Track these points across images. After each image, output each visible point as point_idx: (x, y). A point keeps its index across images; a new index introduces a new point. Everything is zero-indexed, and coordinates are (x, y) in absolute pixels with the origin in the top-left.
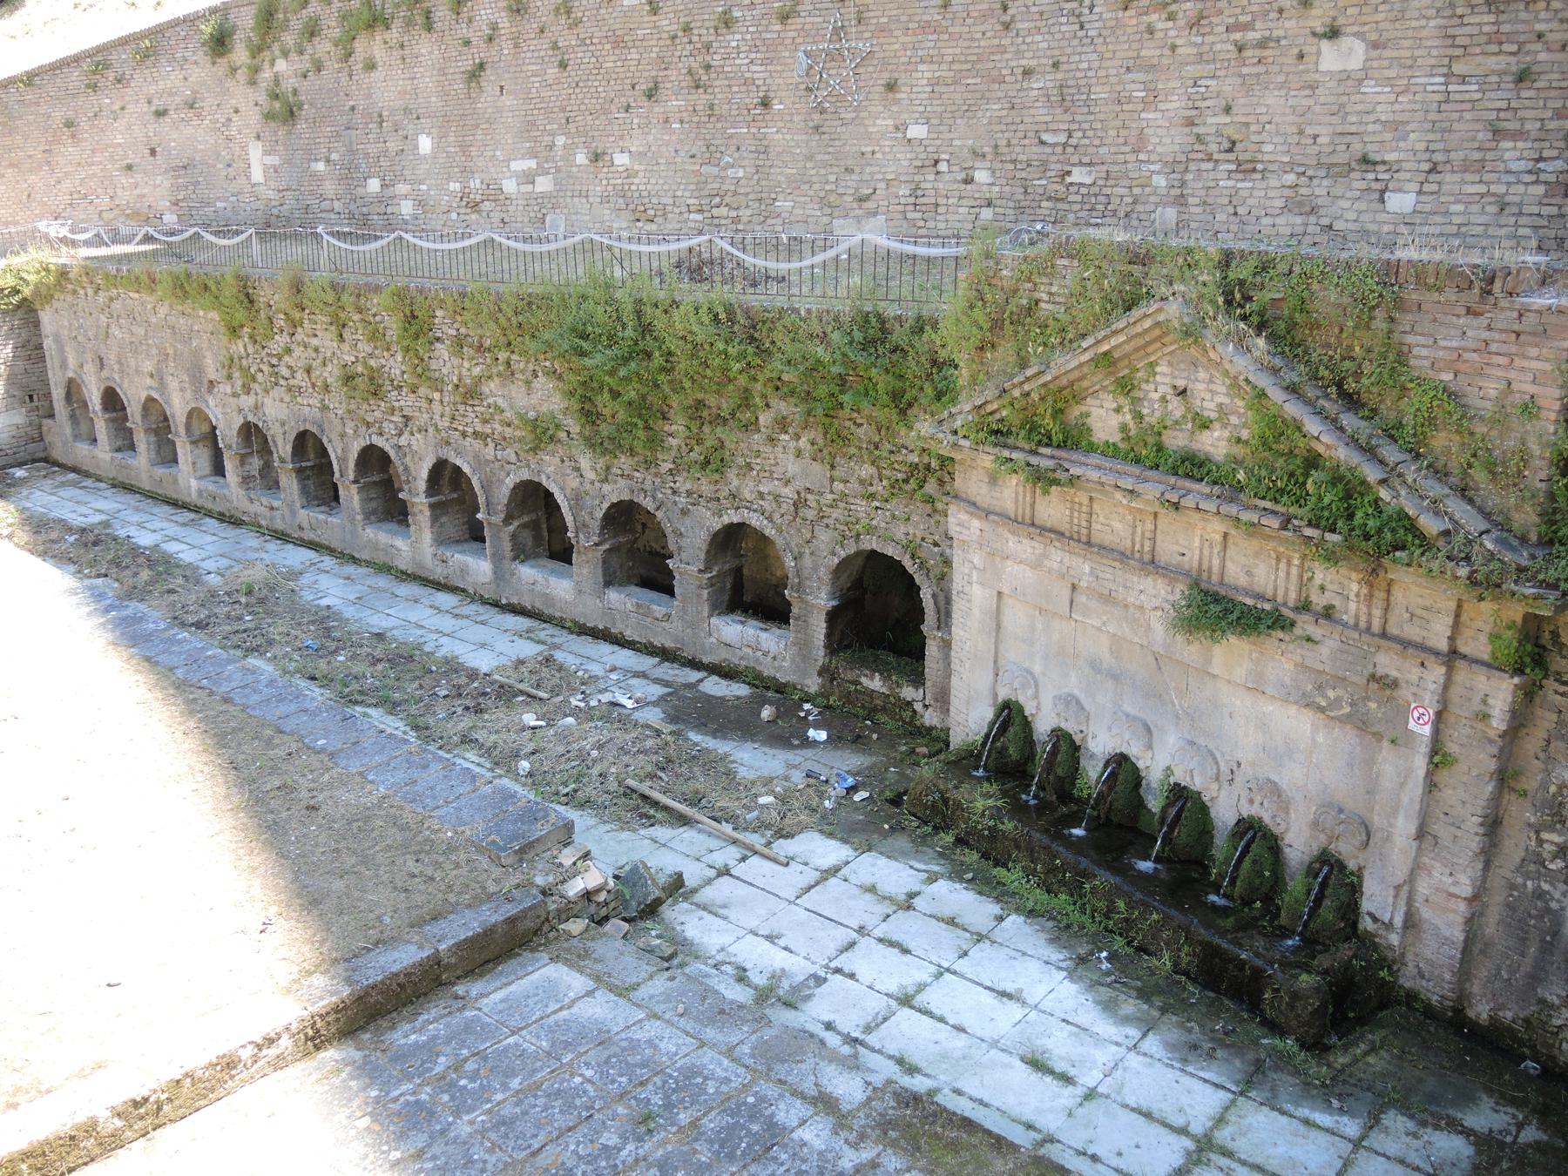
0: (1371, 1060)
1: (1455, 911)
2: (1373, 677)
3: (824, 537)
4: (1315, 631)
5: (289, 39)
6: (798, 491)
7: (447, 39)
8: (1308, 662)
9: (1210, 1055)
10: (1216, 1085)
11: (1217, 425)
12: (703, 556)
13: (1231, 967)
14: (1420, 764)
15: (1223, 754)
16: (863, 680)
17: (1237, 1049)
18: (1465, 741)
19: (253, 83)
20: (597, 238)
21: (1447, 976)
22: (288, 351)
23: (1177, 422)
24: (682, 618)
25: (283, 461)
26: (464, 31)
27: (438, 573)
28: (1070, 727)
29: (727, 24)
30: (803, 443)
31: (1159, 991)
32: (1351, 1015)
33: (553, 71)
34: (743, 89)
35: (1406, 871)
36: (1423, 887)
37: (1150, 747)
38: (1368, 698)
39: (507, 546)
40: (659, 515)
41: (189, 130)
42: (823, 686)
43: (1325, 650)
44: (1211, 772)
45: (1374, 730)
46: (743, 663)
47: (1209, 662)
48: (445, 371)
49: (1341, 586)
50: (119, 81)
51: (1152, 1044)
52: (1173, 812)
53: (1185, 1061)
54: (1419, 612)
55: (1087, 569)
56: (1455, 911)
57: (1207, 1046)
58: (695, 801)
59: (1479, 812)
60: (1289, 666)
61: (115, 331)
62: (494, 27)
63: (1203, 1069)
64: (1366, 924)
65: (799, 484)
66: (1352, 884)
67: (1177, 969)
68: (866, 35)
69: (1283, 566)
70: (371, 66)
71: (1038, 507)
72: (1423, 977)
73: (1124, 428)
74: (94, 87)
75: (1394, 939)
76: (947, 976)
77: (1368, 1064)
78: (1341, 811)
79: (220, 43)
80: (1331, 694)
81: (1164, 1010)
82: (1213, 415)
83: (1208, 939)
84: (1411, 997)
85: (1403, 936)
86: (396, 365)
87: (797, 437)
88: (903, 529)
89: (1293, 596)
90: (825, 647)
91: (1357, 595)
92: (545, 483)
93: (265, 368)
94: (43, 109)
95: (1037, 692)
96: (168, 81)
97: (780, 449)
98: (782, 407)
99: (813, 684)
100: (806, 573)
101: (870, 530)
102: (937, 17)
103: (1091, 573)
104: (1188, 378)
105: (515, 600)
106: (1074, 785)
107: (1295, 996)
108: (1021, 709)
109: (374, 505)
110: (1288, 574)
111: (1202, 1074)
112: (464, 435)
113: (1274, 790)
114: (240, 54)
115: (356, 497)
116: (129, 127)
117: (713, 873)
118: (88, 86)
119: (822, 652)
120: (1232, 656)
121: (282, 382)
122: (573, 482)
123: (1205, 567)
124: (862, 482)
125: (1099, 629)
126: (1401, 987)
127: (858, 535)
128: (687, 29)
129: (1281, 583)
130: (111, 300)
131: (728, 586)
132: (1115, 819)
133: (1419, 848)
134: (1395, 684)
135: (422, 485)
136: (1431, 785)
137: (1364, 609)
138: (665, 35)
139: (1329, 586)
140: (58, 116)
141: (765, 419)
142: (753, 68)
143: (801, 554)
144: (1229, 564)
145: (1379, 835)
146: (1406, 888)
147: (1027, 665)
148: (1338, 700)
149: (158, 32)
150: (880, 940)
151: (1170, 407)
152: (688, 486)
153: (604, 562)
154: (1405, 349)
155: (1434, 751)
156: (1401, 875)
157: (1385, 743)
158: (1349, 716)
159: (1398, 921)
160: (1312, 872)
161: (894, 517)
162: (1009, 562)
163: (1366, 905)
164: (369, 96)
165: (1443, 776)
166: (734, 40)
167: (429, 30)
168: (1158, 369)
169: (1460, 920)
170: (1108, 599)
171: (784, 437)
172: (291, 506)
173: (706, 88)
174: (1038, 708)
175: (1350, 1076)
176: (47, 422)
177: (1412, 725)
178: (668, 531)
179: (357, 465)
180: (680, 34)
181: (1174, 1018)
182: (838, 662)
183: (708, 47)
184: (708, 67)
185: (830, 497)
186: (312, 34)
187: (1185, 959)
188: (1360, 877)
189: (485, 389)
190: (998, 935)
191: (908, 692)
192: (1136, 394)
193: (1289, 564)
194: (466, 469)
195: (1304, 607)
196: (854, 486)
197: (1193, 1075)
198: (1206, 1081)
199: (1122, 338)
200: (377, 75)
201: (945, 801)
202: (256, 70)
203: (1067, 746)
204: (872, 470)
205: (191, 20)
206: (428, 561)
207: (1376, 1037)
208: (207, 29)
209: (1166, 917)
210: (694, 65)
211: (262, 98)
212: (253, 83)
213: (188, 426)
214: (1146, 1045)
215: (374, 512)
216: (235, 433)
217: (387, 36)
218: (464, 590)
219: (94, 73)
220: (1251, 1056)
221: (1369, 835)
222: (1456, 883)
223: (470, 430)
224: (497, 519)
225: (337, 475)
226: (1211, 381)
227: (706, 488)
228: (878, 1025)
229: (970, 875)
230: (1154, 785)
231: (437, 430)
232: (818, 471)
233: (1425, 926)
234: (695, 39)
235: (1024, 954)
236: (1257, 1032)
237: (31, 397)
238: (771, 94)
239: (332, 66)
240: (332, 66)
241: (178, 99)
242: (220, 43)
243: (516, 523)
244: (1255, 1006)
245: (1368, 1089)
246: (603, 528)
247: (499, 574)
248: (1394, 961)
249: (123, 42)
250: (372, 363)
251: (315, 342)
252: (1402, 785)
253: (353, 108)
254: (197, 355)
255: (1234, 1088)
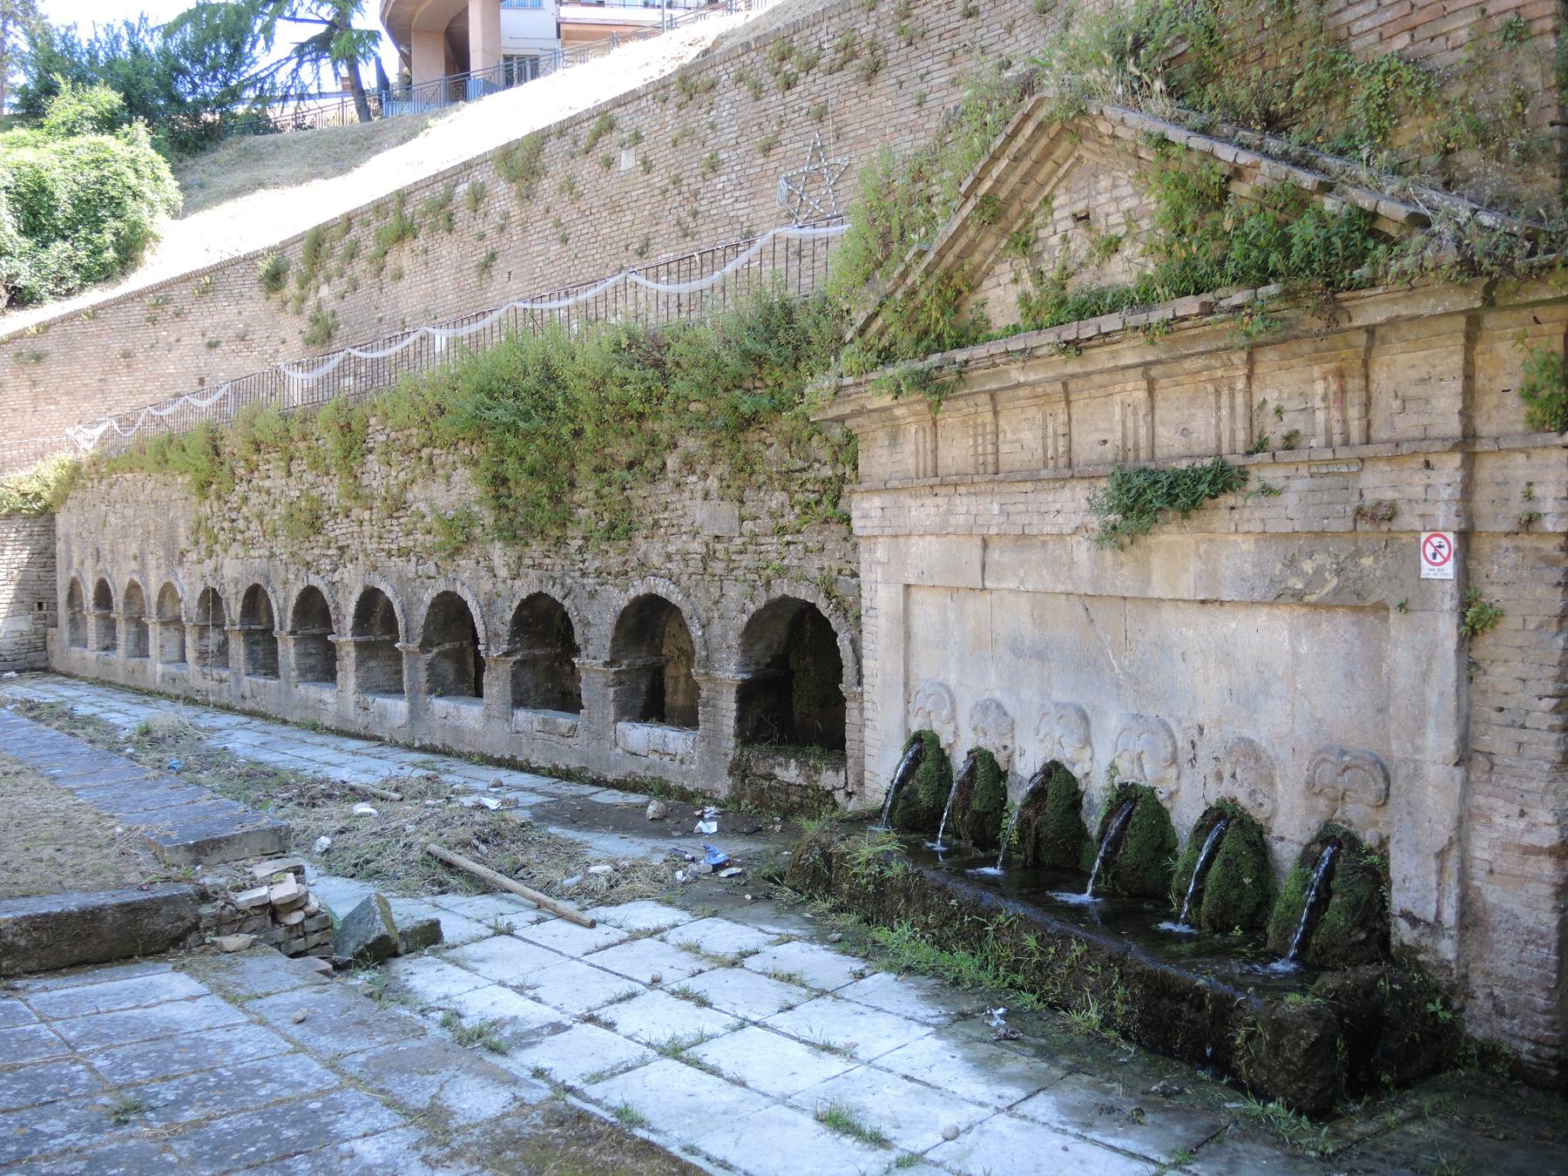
0: (1412, 1129)
1: (1537, 878)
2: (1360, 513)
3: (733, 591)
4: (1273, 475)
5: (332, 265)
6: (702, 544)
7: (466, 237)
8: (1272, 527)
9: (1135, 1119)
10: (1133, 1155)
11: (1127, 243)
12: (608, 644)
13: (1184, 1007)
14: (1446, 629)
15: (1180, 721)
16: (778, 771)
17: (1185, 1115)
18: (1510, 575)
19: (299, 312)
20: (521, 305)
21: (1540, 1001)
22: (246, 499)
23: (1081, 264)
24: (587, 729)
25: (233, 624)
26: (480, 226)
27: (359, 722)
28: (989, 743)
29: (714, 168)
30: (713, 483)
31: (1071, 1048)
32: (1386, 1078)
33: (555, 248)
34: (728, 228)
35: (1450, 821)
36: (1482, 850)
37: (1087, 741)
38: (1359, 553)
39: (423, 676)
40: (567, 603)
41: (239, 361)
42: (734, 788)
43: (1290, 499)
44: (1165, 751)
45: (1374, 599)
46: (649, 774)
47: (1147, 582)
48: (375, 484)
49: (1295, 390)
50: (178, 315)
51: (1042, 1106)
52: (1116, 823)
53: (1089, 1126)
54: (1412, 391)
55: (996, 508)
56: (1537, 878)
57: (1129, 1109)
58: (514, 871)
59: (1550, 688)
60: (1247, 545)
61: (112, 519)
62: (506, 216)
63: (1116, 1135)
64: (1403, 933)
65: (706, 535)
66: (1370, 869)
67: (1107, 1023)
68: (845, 150)
69: (1225, 399)
70: (399, 276)
71: (941, 453)
72: (1500, 1012)
73: (1025, 299)
74: (153, 320)
75: (1447, 948)
76: (752, 1030)
77: (1408, 1134)
78: (1343, 753)
79: (275, 279)
80: (1308, 566)
81: (1071, 1070)
82: (1121, 231)
83: (1150, 966)
84: (1489, 1054)
85: (1461, 942)
86: (333, 491)
87: (706, 475)
88: (817, 564)
89: (1241, 436)
90: (736, 736)
91: (1325, 398)
92: (459, 592)
93: (226, 525)
94: (104, 340)
95: (954, 710)
96: (225, 315)
97: (687, 494)
98: (689, 443)
99: (723, 787)
100: (714, 643)
101: (781, 572)
102: (913, 117)
103: (1001, 512)
104: (1088, 197)
105: (427, 741)
106: (998, 827)
107: (1279, 1028)
108: (935, 740)
109: (311, 661)
110: (1232, 408)
111: (1118, 1143)
112: (390, 554)
113: (1250, 752)
114: (291, 288)
115: (292, 651)
116: (182, 358)
117: (491, 932)
118: (148, 320)
119: (732, 743)
120: (1176, 555)
121: (239, 537)
122: (486, 585)
123: (1130, 445)
124: (772, 515)
125: (1017, 592)
126: (1470, 1040)
127: (768, 583)
128: (677, 181)
129: (1225, 426)
130: (111, 486)
131: (643, 688)
132: (1047, 859)
133: (1466, 781)
134: (1390, 513)
135: (349, 622)
136: (1470, 668)
137: (1335, 414)
138: (657, 192)
139: (1287, 406)
140: (117, 347)
141: (672, 461)
142: (738, 206)
143: (709, 621)
144: (1161, 431)
145: (1402, 772)
146: (1454, 852)
147: (940, 679)
148: (1319, 571)
149: (219, 269)
150: (673, 993)
151: (1073, 246)
152: (597, 564)
153: (514, 676)
154: (1343, 34)
155: (1465, 603)
156: (1442, 832)
157: (1394, 616)
158: (1337, 591)
159: (1450, 916)
160: (1308, 858)
161: (806, 549)
162: (914, 539)
163: (1399, 900)
164: (395, 305)
165: (1486, 647)
166: (719, 182)
167: (450, 231)
168: (1055, 204)
169: (1547, 890)
170: (1023, 539)
171: (693, 479)
172: (236, 675)
173: (693, 235)
174: (956, 734)
175: (1375, 1147)
176: (52, 630)
177: (1427, 571)
178: (574, 621)
179: (295, 613)
180: (671, 187)
181: (1086, 1078)
182: (752, 753)
183: (696, 194)
184: (695, 214)
185: (739, 541)
186: (352, 256)
187: (1121, 1009)
188: (1385, 858)
189: (410, 496)
190: (849, 992)
191: (828, 779)
192: (1037, 247)
193: (1232, 391)
194: (389, 593)
195: (1259, 446)
196: (766, 523)
197: (1095, 1142)
198: (1115, 1149)
199: (1003, 163)
200: (404, 283)
201: (827, 858)
202: (303, 300)
203: (989, 771)
204: (781, 497)
205: (251, 259)
206: (351, 709)
207: (1427, 1104)
208: (264, 266)
209: (1092, 950)
210: (683, 215)
211: (304, 325)
212: (299, 312)
213: (160, 605)
214: (1027, 1108)
215: (311, 669)
216: (196, 603)
217: (415, 244)
218: (380, 739)
219: (155, 306)
220: (1204, 1121)
221: (1387, 779)
222: (1532, 828)
223: (394, 547)
224: (414, 646)
225: (277, 628)
226: (1115, 186)
227: (614, 562)
228: (613, 1075)
229: (837, 936)
230: (1097, 801)
231: (367, 555)
232: (728, 510)
233: (1494, 918)
234: (685, 189)
235: (878, 1010)
236: (1220, 1094)
237: (40, 605)
238: (754, 229)
239: (366, 281)
240: (366, 281)
241: (230, 332)
242: (275, 279)
243: (435, 651)
244: (1222, 1065)
245: (1405, 1164)
246: (514, 634)
247: (414, 713)
248: (1452, 990)
249: (186, 279)
250: (314, 493)
251: (268, 483)
252: (1425, 675)
253: (380, 320)
254: (172, 525)
255: (1164, 1160)
